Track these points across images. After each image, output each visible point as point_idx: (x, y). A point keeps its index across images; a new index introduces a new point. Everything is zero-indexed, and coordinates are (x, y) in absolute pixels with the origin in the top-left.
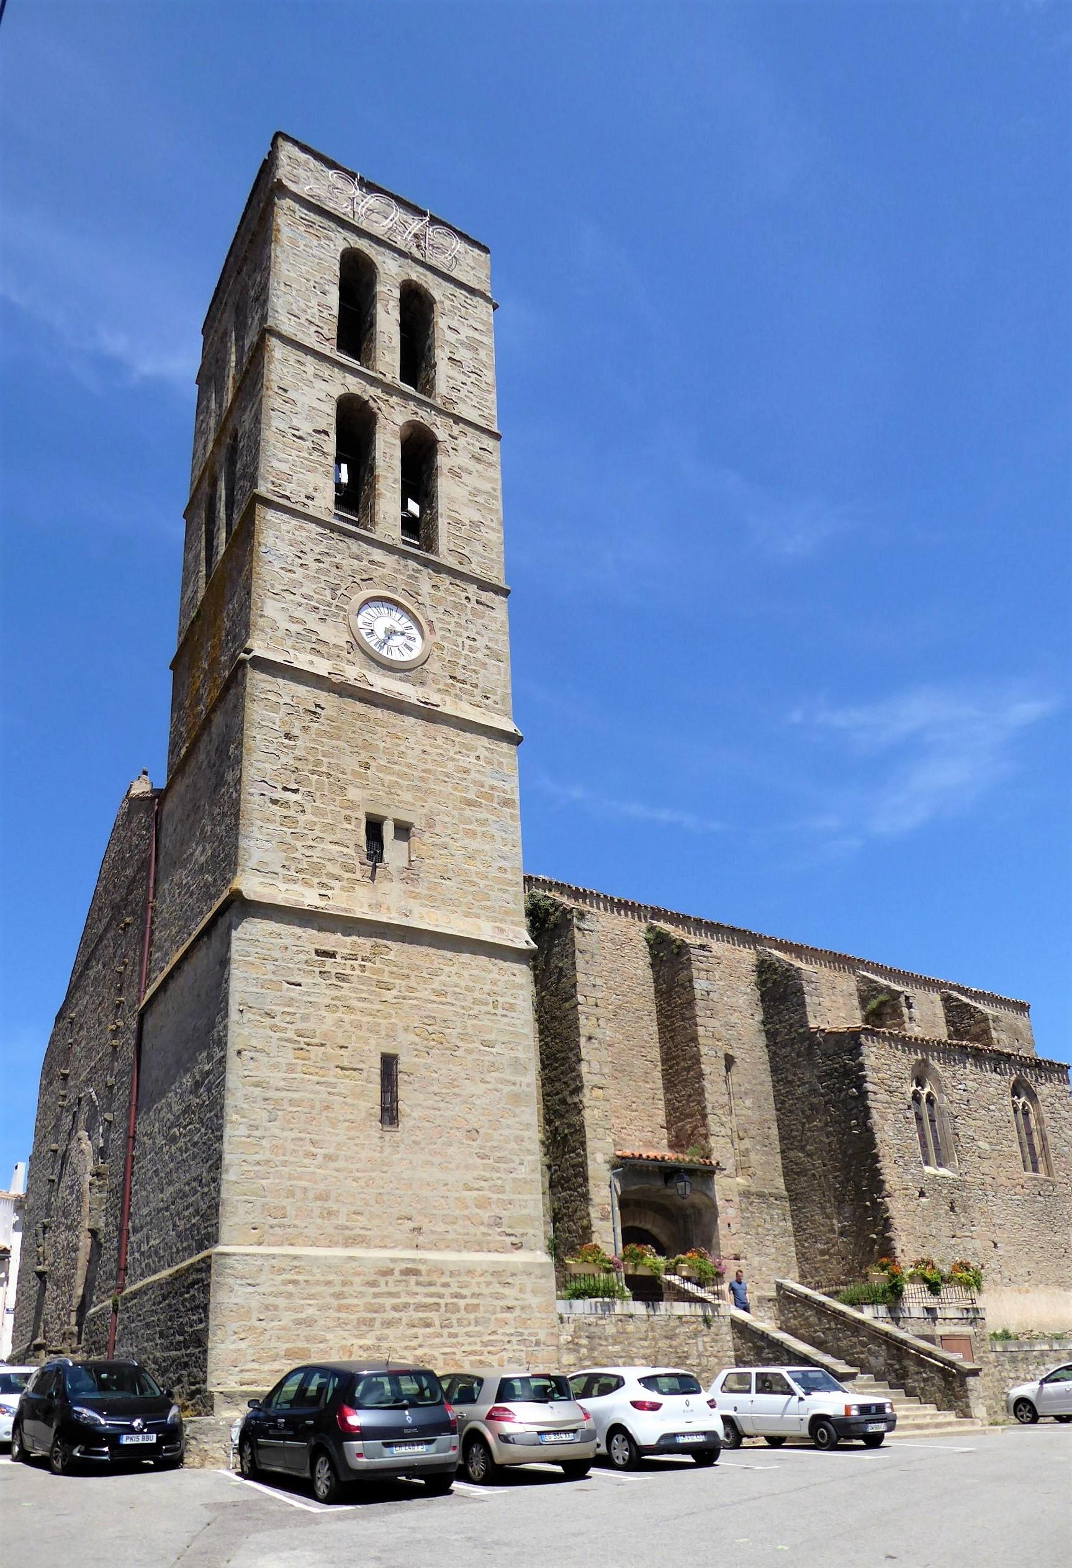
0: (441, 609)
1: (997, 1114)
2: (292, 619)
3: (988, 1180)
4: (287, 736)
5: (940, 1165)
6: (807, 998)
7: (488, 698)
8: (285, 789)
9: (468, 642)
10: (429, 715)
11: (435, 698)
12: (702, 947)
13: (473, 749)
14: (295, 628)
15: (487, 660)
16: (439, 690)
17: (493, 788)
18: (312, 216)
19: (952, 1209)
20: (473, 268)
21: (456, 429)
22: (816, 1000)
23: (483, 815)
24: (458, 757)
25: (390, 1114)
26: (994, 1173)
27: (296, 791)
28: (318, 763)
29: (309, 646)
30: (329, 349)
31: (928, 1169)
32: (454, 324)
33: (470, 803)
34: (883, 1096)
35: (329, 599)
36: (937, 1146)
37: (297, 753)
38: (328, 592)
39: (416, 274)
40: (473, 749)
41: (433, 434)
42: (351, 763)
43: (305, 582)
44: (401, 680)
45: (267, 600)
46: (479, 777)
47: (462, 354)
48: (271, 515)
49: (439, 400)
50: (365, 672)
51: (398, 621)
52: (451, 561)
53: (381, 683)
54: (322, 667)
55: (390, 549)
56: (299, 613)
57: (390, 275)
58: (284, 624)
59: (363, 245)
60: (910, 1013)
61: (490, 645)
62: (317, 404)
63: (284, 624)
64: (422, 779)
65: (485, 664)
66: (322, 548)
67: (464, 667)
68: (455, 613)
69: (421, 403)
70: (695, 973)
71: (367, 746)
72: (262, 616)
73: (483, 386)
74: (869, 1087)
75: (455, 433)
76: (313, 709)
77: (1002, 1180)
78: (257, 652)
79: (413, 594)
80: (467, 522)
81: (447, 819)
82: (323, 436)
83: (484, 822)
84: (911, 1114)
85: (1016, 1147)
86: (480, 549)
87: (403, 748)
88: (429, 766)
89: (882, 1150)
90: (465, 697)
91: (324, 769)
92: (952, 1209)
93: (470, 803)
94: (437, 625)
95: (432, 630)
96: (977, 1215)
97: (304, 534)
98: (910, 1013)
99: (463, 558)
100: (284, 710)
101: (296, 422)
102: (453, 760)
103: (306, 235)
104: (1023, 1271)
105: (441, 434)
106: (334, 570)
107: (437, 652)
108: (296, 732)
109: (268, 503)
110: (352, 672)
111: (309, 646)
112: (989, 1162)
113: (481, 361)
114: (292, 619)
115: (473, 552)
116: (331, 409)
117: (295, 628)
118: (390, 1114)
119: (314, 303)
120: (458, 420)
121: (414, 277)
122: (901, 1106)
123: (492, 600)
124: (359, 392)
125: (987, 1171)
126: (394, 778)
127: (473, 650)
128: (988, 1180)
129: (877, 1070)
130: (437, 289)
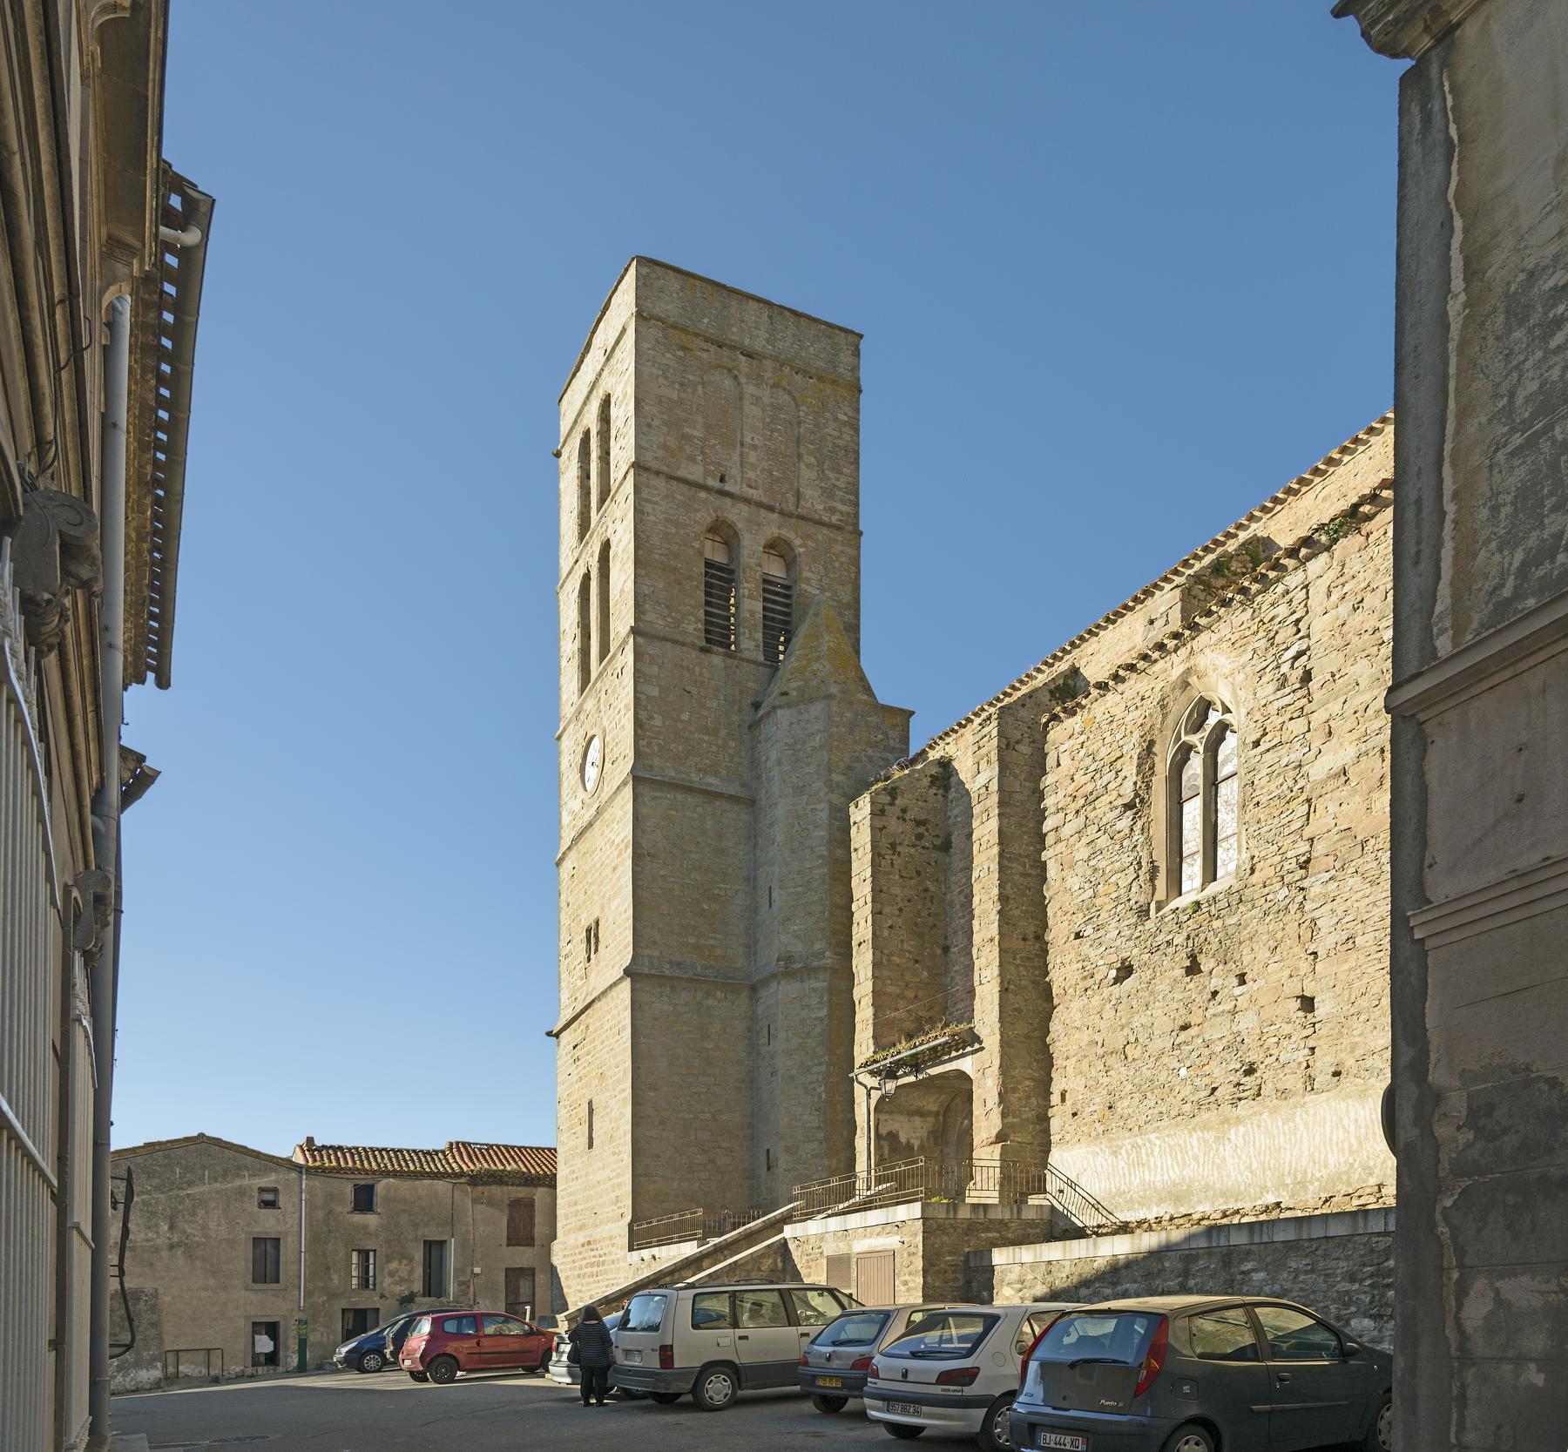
25: (591, 1146)
118: (591, 1146)
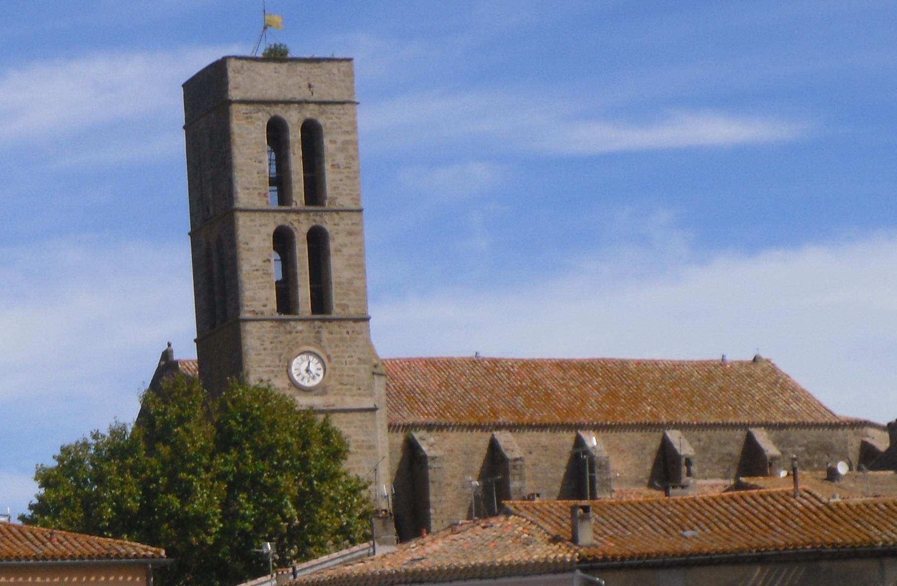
0: (333, 345)
90: (347, 393)
94: (332, 356)
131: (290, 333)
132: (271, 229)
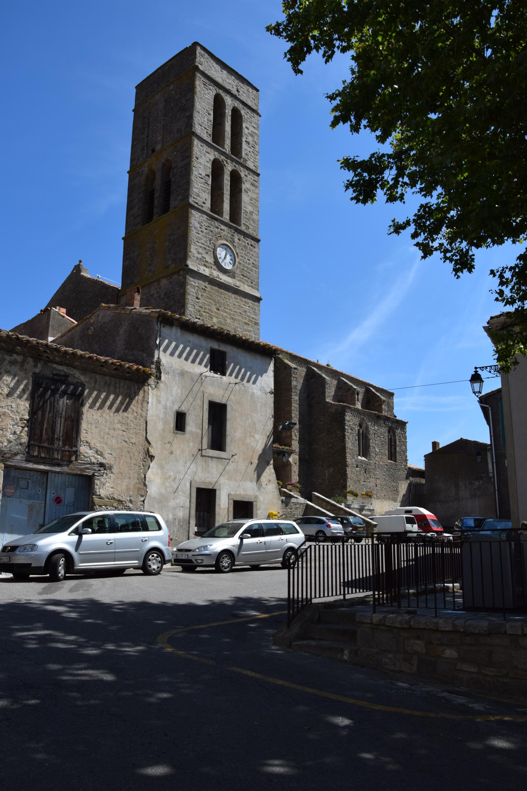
1: (383, 439)
2: (198, 253)
3: (377, 462)
4: (197, 298)
5: (363, 456)
6: (326, 390)
7: (252, 283)
8: (196, 318)
9: (248, 261)
10: (236, 291)
11: (238, 283)
12: (295, 369)
13: (248, 303)
14: (200, 256)
15: (253, 268)
16: (239, 280)
17: (253, 318)
18: (206, 81)
19: (365, 472)
20: (254, 100)
21: (247, 172)
22: (329, 391)
23: (250, 328)
24: (243, 306)
26: (379, 460)
27: (199, 319)
28: (205, 308)
29: (203, 263)
30: (209, 140)
31: (359, 457)
32: (248, 126)
33: (246, 324)
34: (350, 431)
35: (209, 244)
36: (364, 449)
37: (200, 305)
38: (208, 242)
39: (237, 104)
40: (248, 303)
41: (240, 175)
42: (214, 308)
43: (203, 238)
44: (229, 276)
45: (192, 245)
46: (249, 314)
47: (250, 139)
48: (193, 212)
49: (242, 160)
50: (219, 273)
51: (228, 257)
52: (243, 228)
53: (224, 279)
54: (206, 272)
55: (226, 224)
56: (200, 250)
57: (229, 101)
58: (196, 255)
59: (221, 92)
60: (358, 397)
61: (254, 262)
62: (206, 164)
63: (196, 255)
64: (233, 315)
65: (252, 270)
66: (207, 224)
67: (246, 271)
68: (244, 249)
69: (238, 163)
70: (292, 378)
71: (219, 302)
72: (190, 252)
73: (255, 152)
74: (346, 427)
75: (246, 174)
76: (204, 288)
77: (381, 463)
78: (191, 267)
79: (233, 242)
80: (248, 211)
81: (240, 330)
82: (207, 177)
83: (250, 331)
84: (357, 438)
85: (387, 452)
86: (252, 223)
87: (228, 303)
88: (235, 310)
89: (347, 451)
90: (246, 283)
91: (207, 311)
92: (365, 472)
93: (246, 324)
94: (239, 254)
95: (238, 257)
96: (372, 475)
97: (202, 218)
98: (358, 397)
99: (247, 227)
100: (196, 288)
101: (200, 172)
102: (242, 307)
103: (204, 88)
104: (383, 495)
105: (242, 175)
106: (210, 233)
107: (239, 265)
108: (199, 297)
109: (193, 207)
110: (216, 273)
111: (203, 263)
112: (378, 456)
113: (255, 141)
114: (198, 253)
115: (250, 224)
116: (210, 165)
117: (200, 256)
119: (206, 120)
120: (248, 169)
121: (236, 106)
122: (355, 435)
123: (255, 244)
124: (219, 158)
125: (377, 459)
126: (225, 314)
127: (249, 264)
128: (377, 462)
129: (349, 421)
130: (244, 112)
131: (217, 228)
132: (212, 158)
